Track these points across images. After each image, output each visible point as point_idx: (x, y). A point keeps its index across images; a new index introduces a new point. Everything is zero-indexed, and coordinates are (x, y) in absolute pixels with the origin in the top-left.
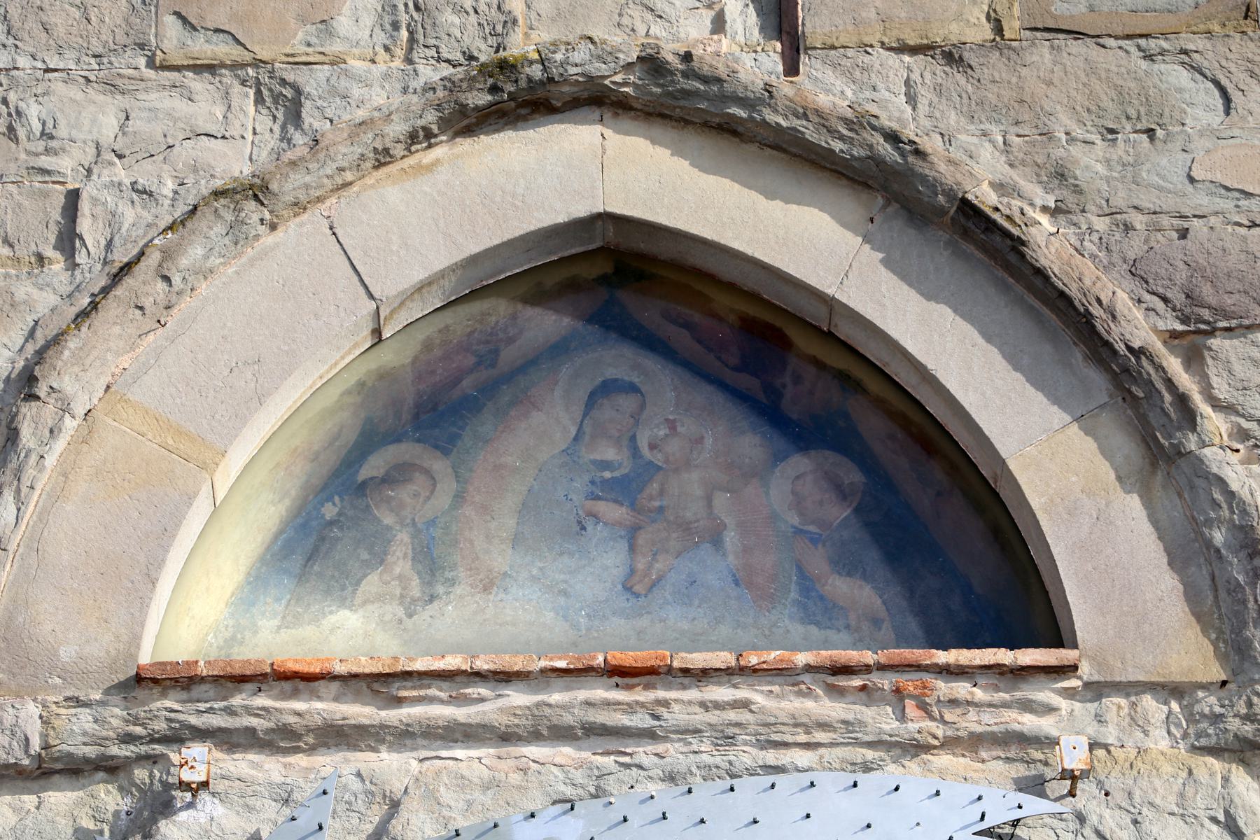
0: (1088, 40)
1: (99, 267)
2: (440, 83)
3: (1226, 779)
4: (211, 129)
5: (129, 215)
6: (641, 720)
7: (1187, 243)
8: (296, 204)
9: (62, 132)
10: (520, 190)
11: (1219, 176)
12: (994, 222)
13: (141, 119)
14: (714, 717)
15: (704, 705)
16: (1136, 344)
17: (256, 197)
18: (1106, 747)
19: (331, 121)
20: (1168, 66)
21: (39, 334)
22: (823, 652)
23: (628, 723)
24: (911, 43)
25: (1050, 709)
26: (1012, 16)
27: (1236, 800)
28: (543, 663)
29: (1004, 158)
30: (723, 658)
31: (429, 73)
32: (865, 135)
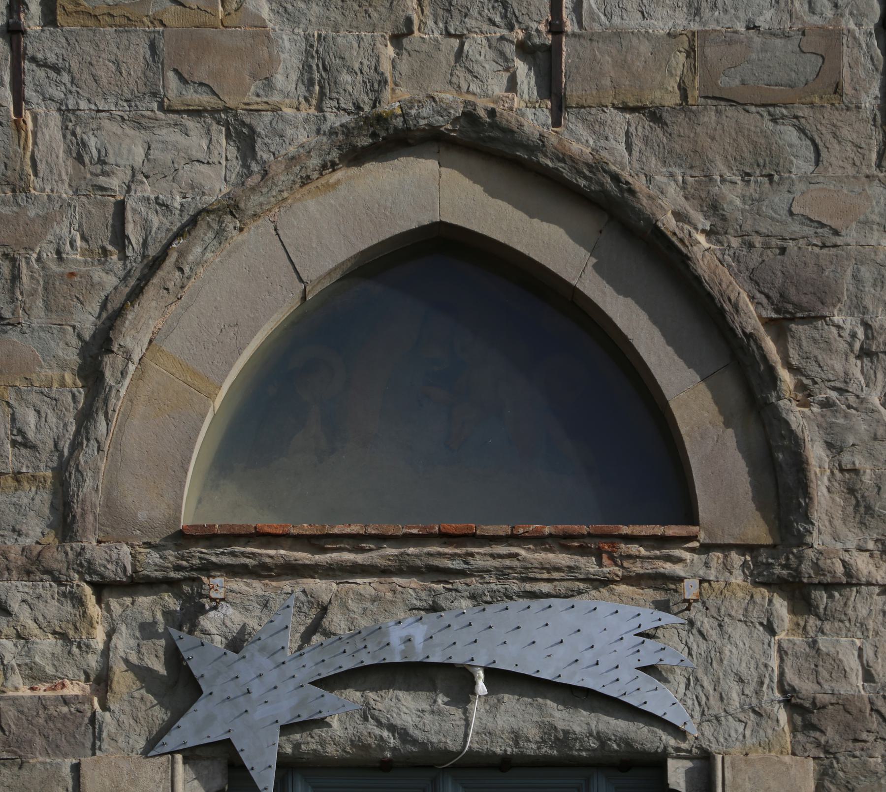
0: (739, 107)
1: (139, 259)
2: (340, 128)
3: (770, 601)
4: (201, 156)
5: (155, 221)
6: (457, 564)
7: (785, 258)
8: (255, 215)
9: (111, 159)
10: (389, 204)
11: (807, 211)
12: (672, 243)
13: (157, 149)
14: (497, 563)
15: (493, 556)
16: (749, 330)
17: (231, 213)
18: (709, 581)
19: (274, 154)
20: (786, 128)
21: (109, 306)
22: (559, 526)
23: (452, 566)
24: (631, 105)
25: (679, 560)
26: (694, 87)
27: (774, 613)
28: (405, 530)
29: (682, 193)
30: (503, 529)
31: (334, 119)
32: (600, 176)
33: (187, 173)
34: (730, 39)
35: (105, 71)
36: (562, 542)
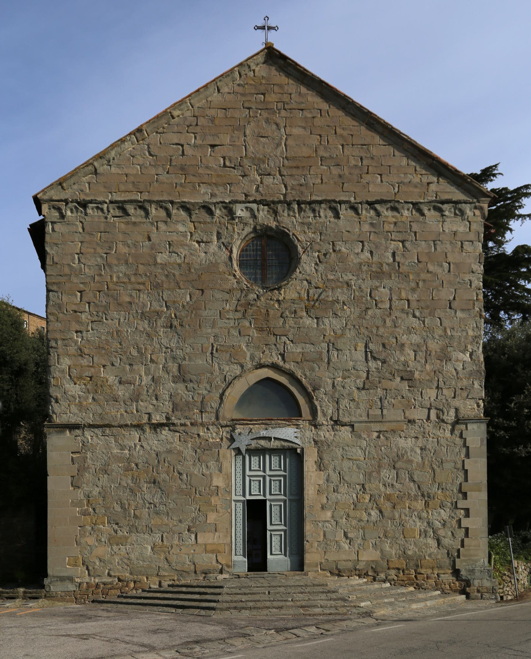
31: (254, 364)
33: (234, 371)
34: (308, 353)
35: (224, 358)
36: (284, 420)
